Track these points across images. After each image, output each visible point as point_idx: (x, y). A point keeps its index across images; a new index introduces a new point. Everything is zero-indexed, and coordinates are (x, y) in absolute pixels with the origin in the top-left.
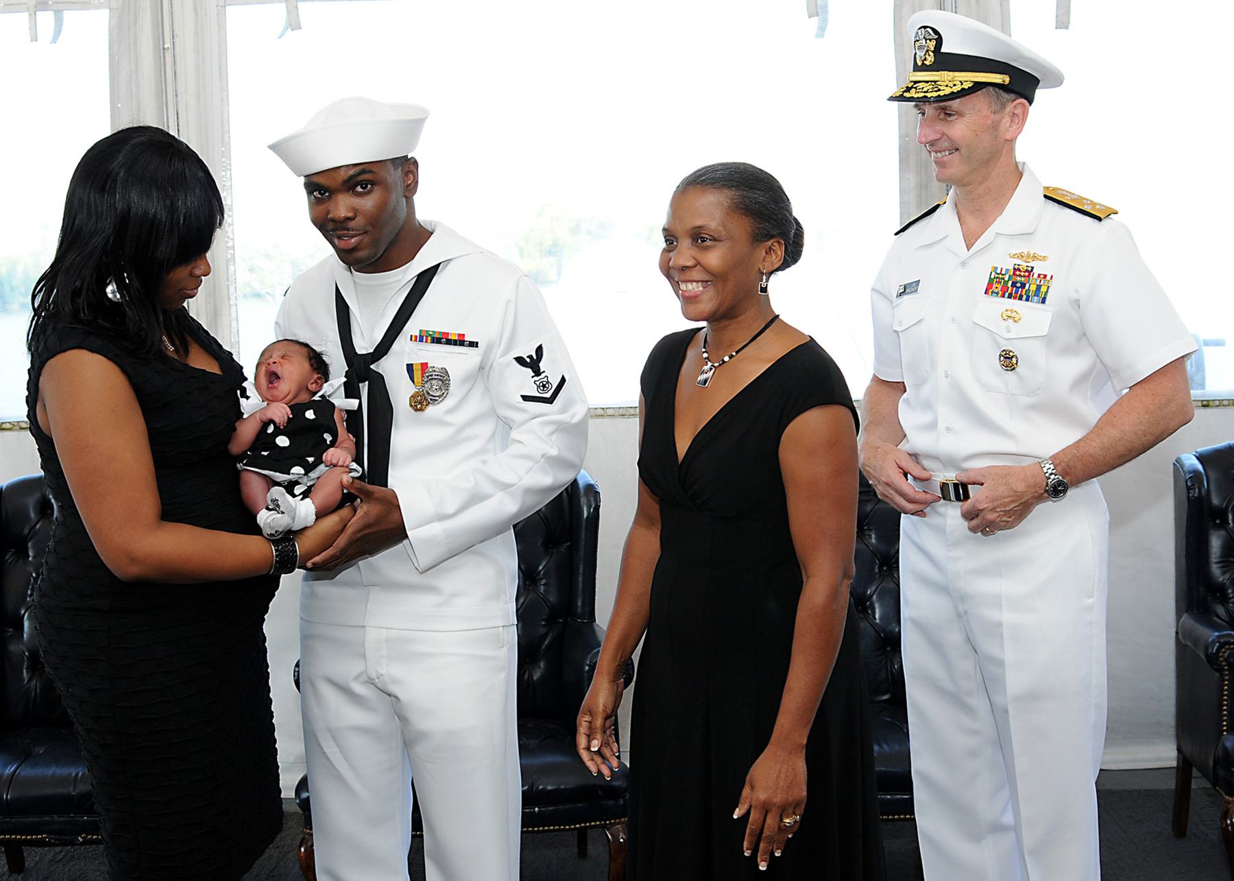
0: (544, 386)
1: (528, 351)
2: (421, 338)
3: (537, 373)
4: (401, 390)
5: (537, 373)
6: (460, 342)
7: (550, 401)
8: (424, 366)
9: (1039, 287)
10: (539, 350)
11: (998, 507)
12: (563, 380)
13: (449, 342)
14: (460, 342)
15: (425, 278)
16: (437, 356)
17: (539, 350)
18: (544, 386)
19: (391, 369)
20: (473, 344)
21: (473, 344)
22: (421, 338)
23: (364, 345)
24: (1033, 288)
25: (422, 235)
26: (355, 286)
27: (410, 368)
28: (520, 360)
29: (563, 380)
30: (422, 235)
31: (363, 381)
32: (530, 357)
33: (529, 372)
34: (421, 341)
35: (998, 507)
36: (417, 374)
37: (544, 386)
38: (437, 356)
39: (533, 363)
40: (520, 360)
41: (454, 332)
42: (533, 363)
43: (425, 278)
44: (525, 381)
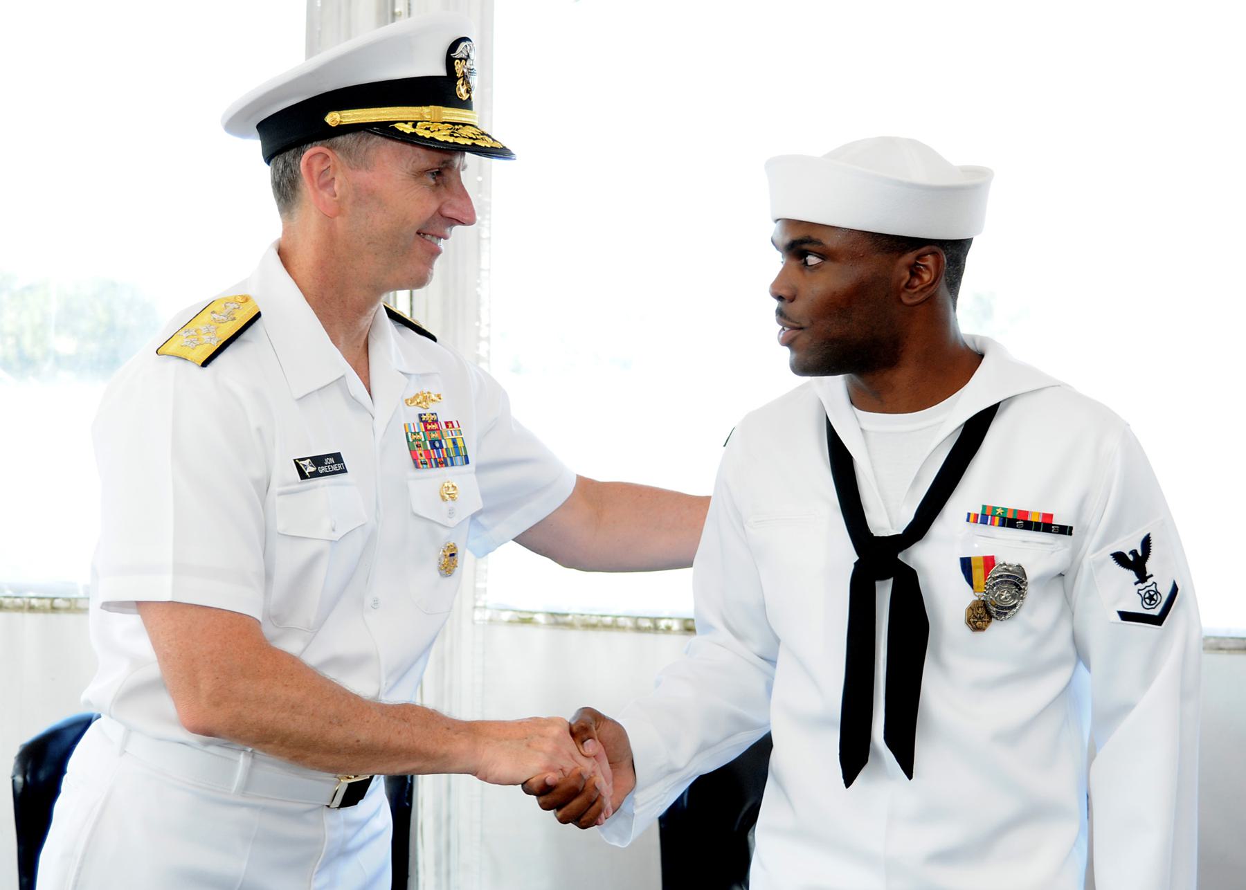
0: (1151, 598)
1: (1130, 544)
2: (985, 517)
3: (1142, 576)
4: (947, 596)
5: (1142, 576)
6: (1046, 526)
7: (1158, 620)
8: (989, 562)
9: (454, 442)
10: (1146, 543)
11: (544, 752)
12: (1175, 590)
13: (1028, 526)
14: (1046, 526)
15: (974, 432)
16: (1012, 548)
17: (1146, 543)
18: (1151, 598)
19: (937, 562)
20: (1065, 530)
21: (1065, 530)
22: (985, 517)
23: (887, 518)
24: (451, 445)
25: (968, 361)
26: (868, 434)
27: (966, 565)
28: (1120, 558)
29: (1175, 590)
30: (968, 361)
31: (884, 577)
32: (1134, 553)
33: (1131, 575)
34: (984, 522)
35: (544, 752)
36: (978, 573)
37: (1151, 598)
38: (1012, 548)
39: (1136, 563)
40: (1120, 558)
41: (1036, 511)
42: (1136, 563)
43: (974, 432)
44: (1124, 591)
